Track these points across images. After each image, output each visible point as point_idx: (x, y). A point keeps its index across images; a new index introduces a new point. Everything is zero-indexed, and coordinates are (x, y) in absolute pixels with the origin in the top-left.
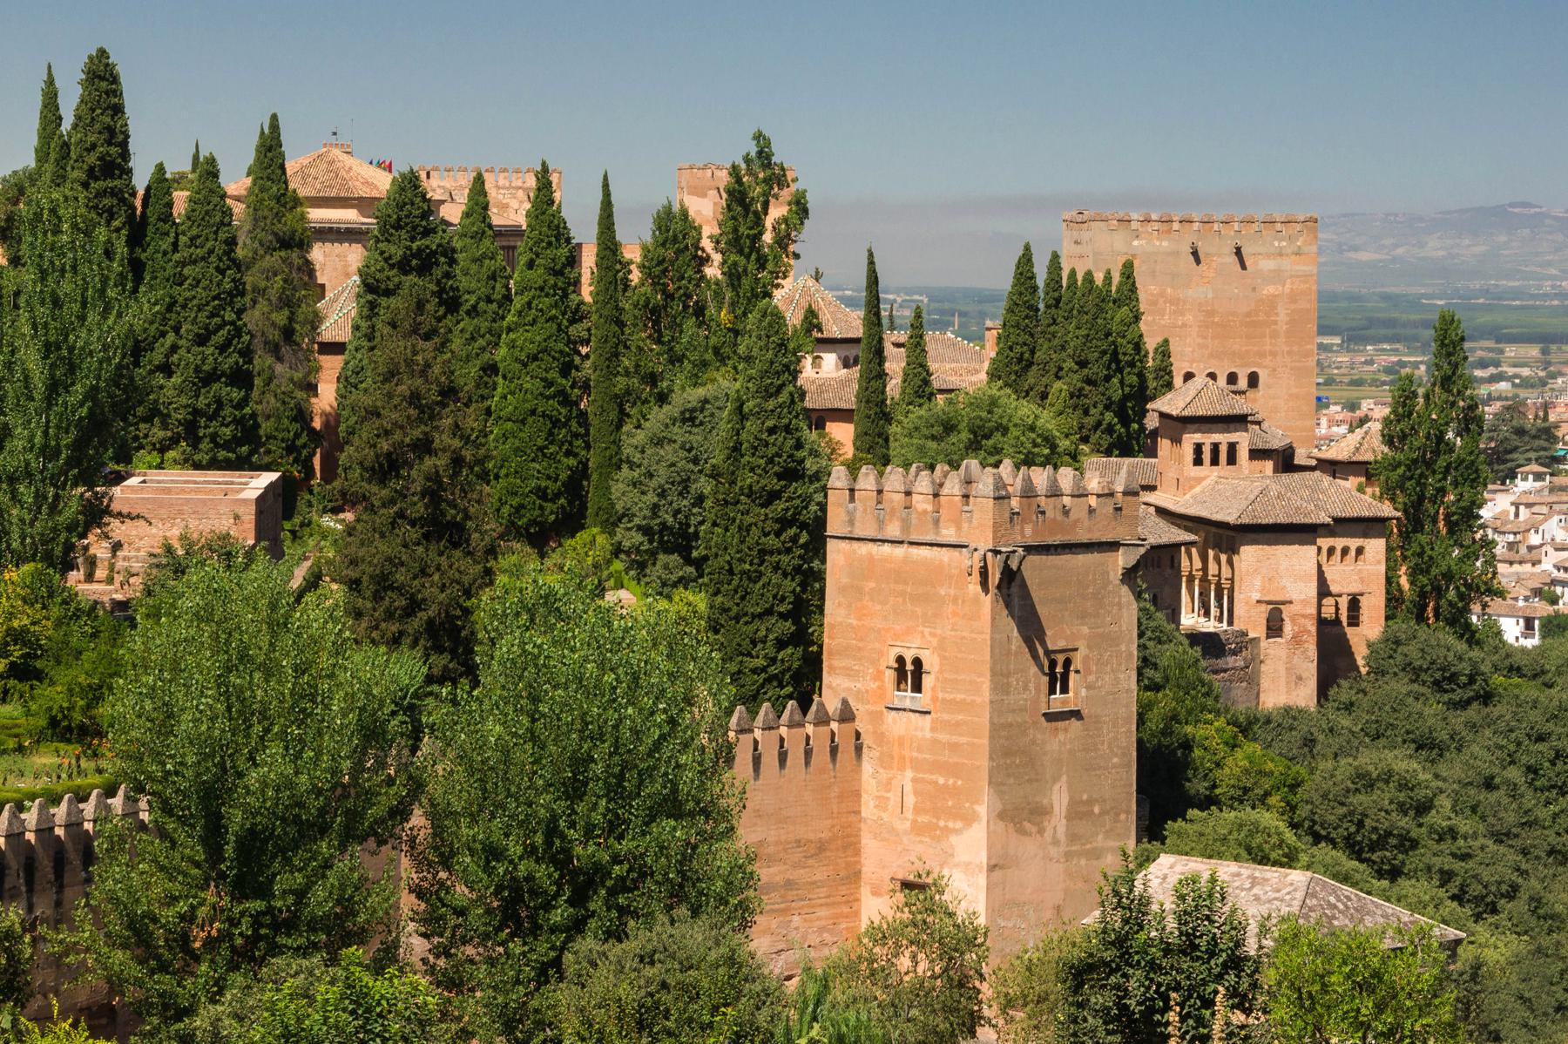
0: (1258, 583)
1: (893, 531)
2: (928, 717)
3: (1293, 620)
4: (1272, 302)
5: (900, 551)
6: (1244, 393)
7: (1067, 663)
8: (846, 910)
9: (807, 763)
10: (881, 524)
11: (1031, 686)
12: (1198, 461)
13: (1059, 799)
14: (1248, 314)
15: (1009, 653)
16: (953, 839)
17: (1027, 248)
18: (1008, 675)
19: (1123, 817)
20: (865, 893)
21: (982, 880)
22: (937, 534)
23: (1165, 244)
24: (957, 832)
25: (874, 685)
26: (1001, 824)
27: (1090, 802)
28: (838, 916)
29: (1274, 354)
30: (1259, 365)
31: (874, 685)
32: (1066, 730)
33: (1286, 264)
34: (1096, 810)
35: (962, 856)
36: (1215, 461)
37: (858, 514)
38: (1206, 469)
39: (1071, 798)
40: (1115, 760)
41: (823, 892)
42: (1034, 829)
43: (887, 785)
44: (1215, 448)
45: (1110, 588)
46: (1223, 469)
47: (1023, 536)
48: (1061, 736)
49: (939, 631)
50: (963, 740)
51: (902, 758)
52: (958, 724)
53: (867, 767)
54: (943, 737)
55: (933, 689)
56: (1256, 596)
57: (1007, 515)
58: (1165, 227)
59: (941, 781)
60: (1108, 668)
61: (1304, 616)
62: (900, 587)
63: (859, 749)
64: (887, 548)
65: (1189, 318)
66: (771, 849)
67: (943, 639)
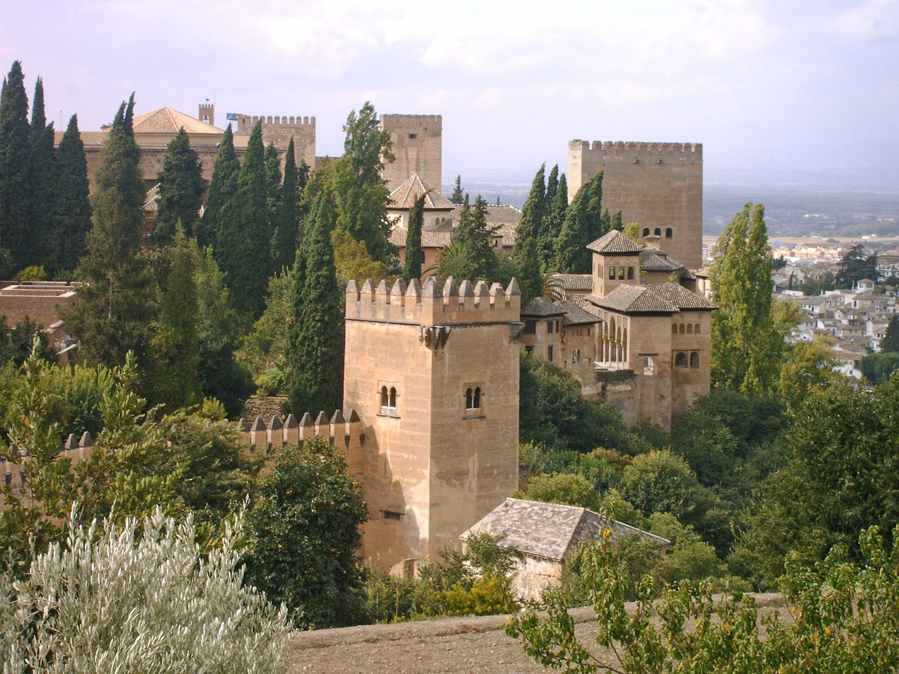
1: (381, 316)
5: (384, 328)
10: (374, 313)
11: (456, 403)
13: (473, 464)
14: (666, 197)
15: (442, 384)
19: (511, 476)
21: (427, 512)
22: (403, 318)
23: (621, 158)
24: (415, 485)
27: (492, 468)
29: (679, 218)
34: (495, 472)
35: (416, 498)
37: (362, 307)
40: (506, 445)
42: (458, 483)
45: (503, 348)
47: (451, 320)
50: (417, 433)
52: (414, 425)
54: (407, 432)
57: (441, 307)
59: (406, 456)
64: (377, 326)
65: (634, 198)
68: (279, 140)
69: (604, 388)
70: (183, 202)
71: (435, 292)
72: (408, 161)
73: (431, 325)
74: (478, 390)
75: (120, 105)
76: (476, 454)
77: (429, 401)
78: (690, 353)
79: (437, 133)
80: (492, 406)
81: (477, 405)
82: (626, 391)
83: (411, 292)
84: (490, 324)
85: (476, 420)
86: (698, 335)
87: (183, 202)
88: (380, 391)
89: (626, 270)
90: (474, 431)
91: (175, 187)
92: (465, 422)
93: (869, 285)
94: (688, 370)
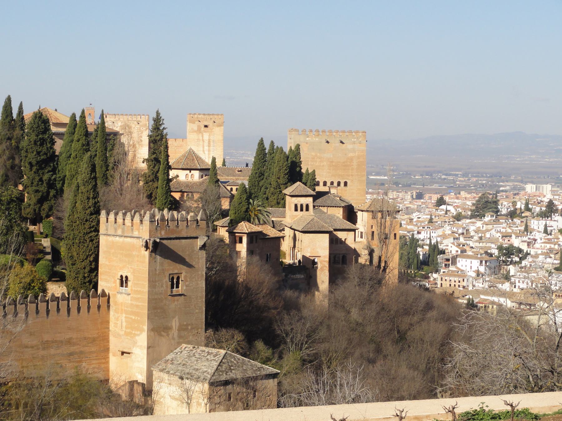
0: (309, 250)
2: (130, 296)
3: (321, 263)
4: (351, 159)
5: (122, 239)
7: (178, 278)
8: (103, 361)
9: (89, 311)
10: (116, 232)
11: (164, 286)
12: (296, 210)
13: (175, 323)
14: (344, 163)
16: (137, 338)
17: (262, 139)
18: (156, 281)
20: (111, 355)
22: (133, 233)
23: (317, 139)
24: (138, 335)
25: (114, 285)
26: (152, 333)
27: (187, 325)
28: (99, 363)
29: (352, 175)
30: (348, 179)
31: (114, 285)
32: (178, 300)
34: (189, 328)
37: (109, 227)
38: (299, 213)
39: (180, 324)
40: (197, 311)
41: (94, 355)
43: (117, 319)
44: (302, 205)
46: (304, 212)
47: (161, 234)
48: (176, 303)
49: (133, 267)
50: (140, 304)
51: (122, 310)
53: (112, 312)
54: (134, 303)
55: (131, 286)
59: (133, 318)
60: (194, 280)
61: (324, 261)
62: (121, 252)
63: (109, 307)
64: (117, 238)
65: (325, 163)
66: (75, 340)
69: (286, 276)
71: (151, 218)
72: (203, 141)
73: (148, 238)
76: (177, 317)
77: (146, 284)
78: (341, 256)
83: (137, 218)
88: (120, 278)
93: (492, 216)
94: (340, 266)
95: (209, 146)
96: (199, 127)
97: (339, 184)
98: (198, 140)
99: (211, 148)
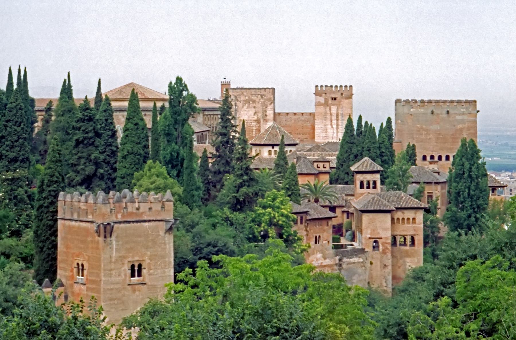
0: (369, 231)
1: (75, 217)
6: (437, 162)
10: (72, 215)
11: (122, 275)
14: (453, 134)
15: (111, 262)
18: (111, 270)
22: (87, 217)
23: (422, 110)
31: (71, 274)
33: (465, 117)
36: (368, 188)
38: (365, 190)
44: (368, 183)
46: (371, 190)
49: (88, 254)
55: (87, 276)
56: (369, 236)
58: (422, 104)
61: (387, 243)
64: (74, 223)
65: (431, 136)
67: (89, 257)
68: (251, 102)
69: (340, 260)
70: (85, 142)
72: (331, 114)
74: (140, 266)
75: (63, 81)
79: (350, 96)
80: (151, 276)
81: (139, 275)
82: (359, 262)
84: (150, 221)
85: (138, 286)
86: (414, 225)
87: (85, 142)
89: (371, 183)
90: (137, 293)
91: (81, 132)
92: (130, 287)
95: (337, 120)
96: (326, 100)
97: (440, 158)
98: (326, 113)
99: (340, 122)
